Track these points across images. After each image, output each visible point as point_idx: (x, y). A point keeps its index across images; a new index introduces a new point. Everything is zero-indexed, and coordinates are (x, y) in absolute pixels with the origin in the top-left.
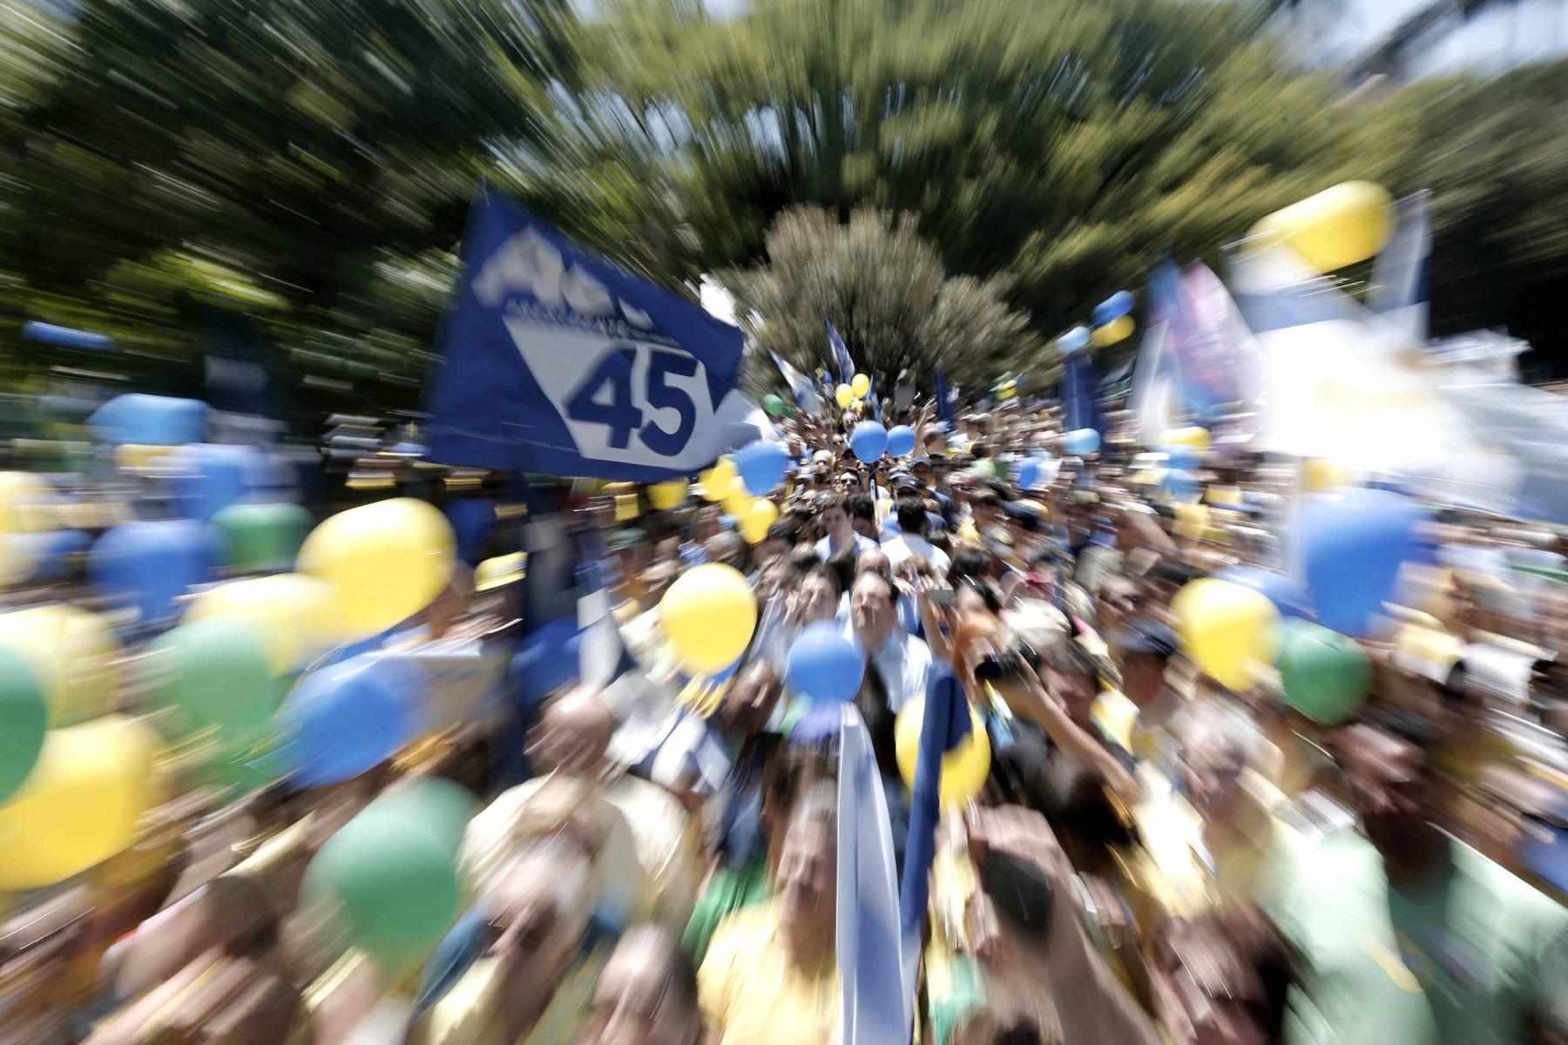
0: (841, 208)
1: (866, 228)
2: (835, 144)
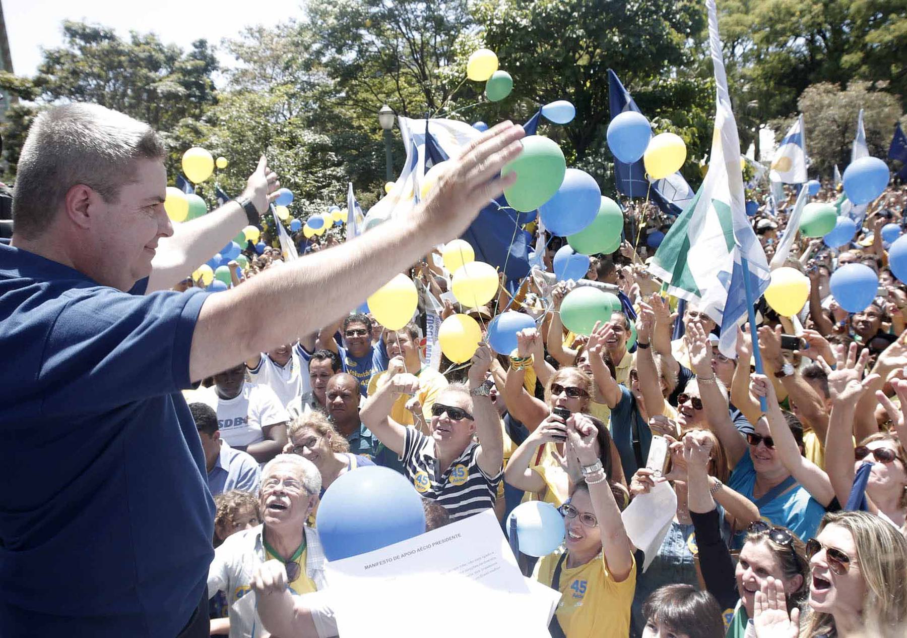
0: (841, 79)
1: (857, 88)
2: (838, 47)
